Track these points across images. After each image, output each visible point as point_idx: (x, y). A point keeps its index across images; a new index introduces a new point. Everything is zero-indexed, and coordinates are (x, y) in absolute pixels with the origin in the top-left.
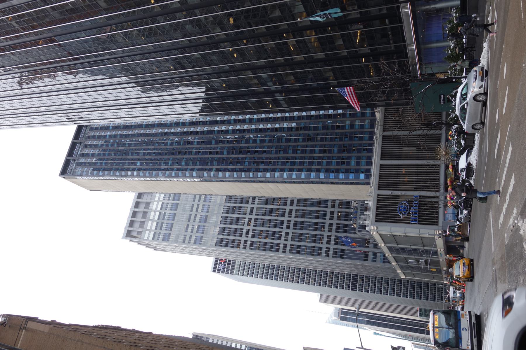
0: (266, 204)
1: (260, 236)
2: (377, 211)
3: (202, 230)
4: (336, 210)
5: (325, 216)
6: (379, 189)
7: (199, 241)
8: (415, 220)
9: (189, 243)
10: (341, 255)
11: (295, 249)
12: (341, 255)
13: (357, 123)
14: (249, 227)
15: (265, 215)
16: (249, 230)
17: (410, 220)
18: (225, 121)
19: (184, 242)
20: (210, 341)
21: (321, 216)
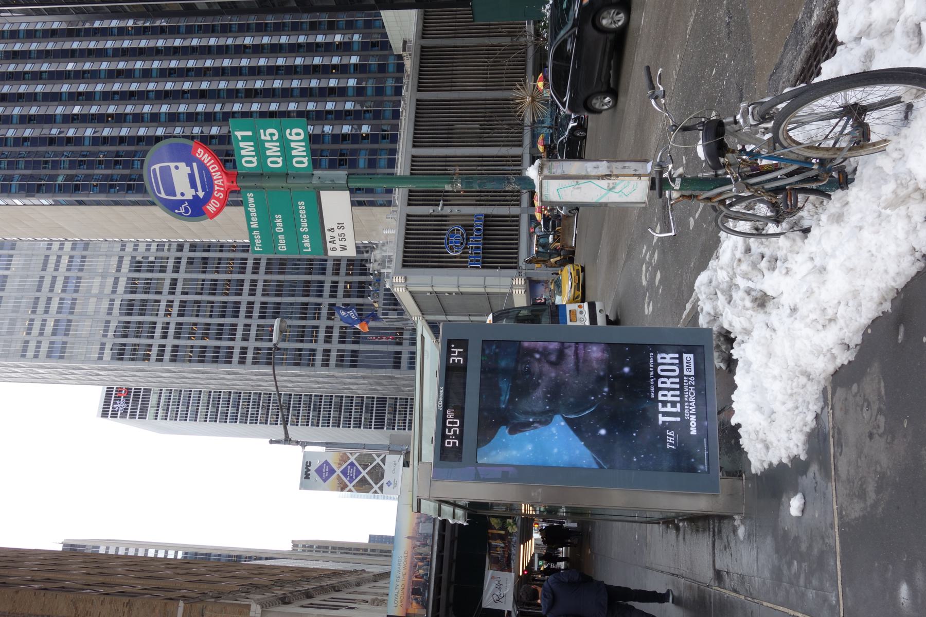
0: (204, 272)
1: (191, 335)
2: (405, 247)
3: (65, 328)
4: (342, 278)
5: (322, 291)
6: (409, 205)
7: (58, 353)
8: (477, 261)
9: (36, 356)
10: (352, 361)
11: (263, 356)
12: (353, 361)
13: (370, 84)
14: (167, 319)
15: (201, 294)
16: (168, 323)
17: (467, 262)
18: (85, 72)
19: (23, 356)
20: (102, 551)
21: (313, 291)
